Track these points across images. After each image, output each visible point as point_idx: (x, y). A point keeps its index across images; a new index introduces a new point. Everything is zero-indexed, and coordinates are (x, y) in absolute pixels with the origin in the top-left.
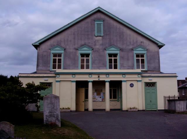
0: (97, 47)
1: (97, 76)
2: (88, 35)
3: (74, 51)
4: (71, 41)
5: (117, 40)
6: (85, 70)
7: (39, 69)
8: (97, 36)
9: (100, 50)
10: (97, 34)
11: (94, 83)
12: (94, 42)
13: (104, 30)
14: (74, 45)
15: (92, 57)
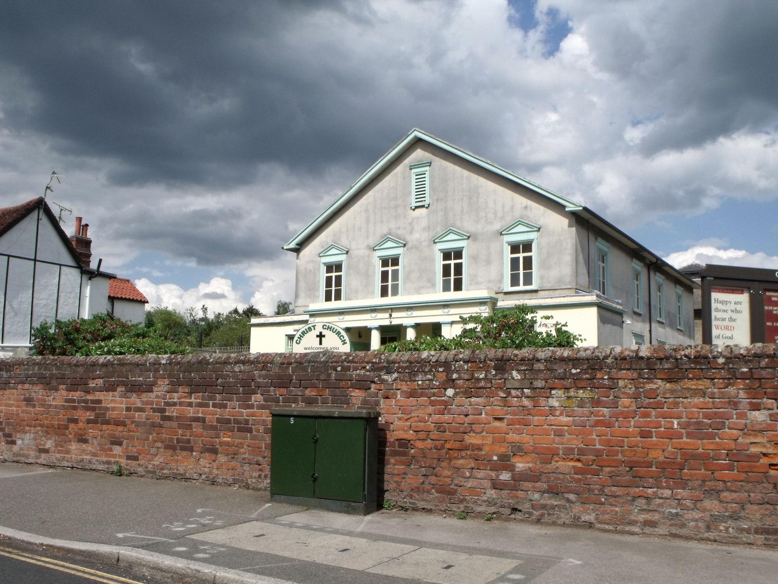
0: (416, 236)
1: (387, 315)
2: (396, 207)
3: (367, 252)
4: (360, 229)
5: (462, 211)
6: (334, 304)
7: (299, 304)
8: (417, 207)
9: (421, 242)
10: (416, 199)
11: (383, 329)
12: (410, 224)
13: (431, 187)
14: (367, 237)
15: (405, 264)
